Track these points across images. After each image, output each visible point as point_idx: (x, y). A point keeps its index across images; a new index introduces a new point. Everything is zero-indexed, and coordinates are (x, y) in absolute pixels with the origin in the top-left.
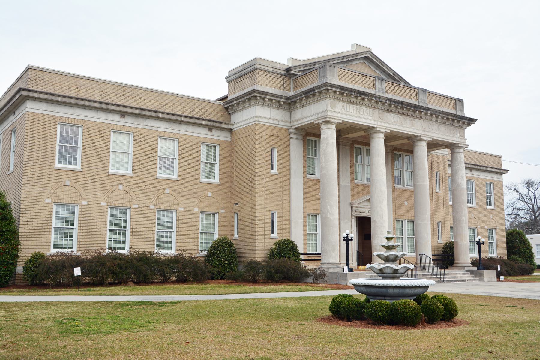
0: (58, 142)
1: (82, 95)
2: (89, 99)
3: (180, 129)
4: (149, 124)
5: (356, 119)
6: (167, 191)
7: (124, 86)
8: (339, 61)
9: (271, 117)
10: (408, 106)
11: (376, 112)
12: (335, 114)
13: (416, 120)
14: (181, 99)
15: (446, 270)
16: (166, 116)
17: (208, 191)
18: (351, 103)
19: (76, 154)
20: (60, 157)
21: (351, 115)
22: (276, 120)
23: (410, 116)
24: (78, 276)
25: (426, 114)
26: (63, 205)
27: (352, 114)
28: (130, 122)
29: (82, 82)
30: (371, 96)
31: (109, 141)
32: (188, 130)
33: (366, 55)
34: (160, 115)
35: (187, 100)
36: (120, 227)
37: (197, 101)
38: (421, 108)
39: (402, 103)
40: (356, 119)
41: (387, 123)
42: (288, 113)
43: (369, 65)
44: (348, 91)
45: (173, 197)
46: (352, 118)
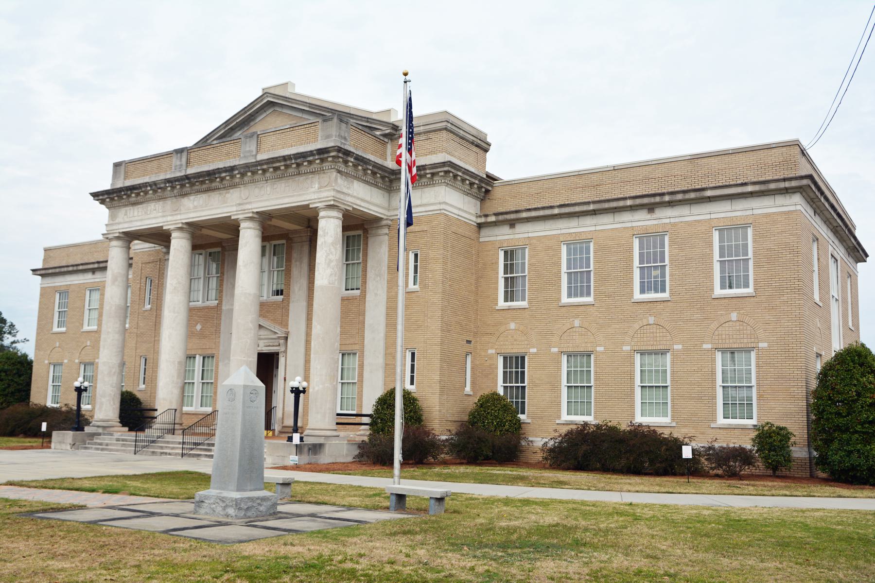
0: (564, 268)
5: (139, 223)
10: (199, 177)
11: (169, 202)
13: (231, 191)
15: (139, 434)
18: (134, 204)
19: (746, 269)
25: (232, 177)
26: (650, 353)
29: (71, 249)
33: (265, 101)
36: (517, 382)
38: (220, 173)
40: (139, 223)
42: (386, 195)
43: (257, 120)
44: (116, 192)
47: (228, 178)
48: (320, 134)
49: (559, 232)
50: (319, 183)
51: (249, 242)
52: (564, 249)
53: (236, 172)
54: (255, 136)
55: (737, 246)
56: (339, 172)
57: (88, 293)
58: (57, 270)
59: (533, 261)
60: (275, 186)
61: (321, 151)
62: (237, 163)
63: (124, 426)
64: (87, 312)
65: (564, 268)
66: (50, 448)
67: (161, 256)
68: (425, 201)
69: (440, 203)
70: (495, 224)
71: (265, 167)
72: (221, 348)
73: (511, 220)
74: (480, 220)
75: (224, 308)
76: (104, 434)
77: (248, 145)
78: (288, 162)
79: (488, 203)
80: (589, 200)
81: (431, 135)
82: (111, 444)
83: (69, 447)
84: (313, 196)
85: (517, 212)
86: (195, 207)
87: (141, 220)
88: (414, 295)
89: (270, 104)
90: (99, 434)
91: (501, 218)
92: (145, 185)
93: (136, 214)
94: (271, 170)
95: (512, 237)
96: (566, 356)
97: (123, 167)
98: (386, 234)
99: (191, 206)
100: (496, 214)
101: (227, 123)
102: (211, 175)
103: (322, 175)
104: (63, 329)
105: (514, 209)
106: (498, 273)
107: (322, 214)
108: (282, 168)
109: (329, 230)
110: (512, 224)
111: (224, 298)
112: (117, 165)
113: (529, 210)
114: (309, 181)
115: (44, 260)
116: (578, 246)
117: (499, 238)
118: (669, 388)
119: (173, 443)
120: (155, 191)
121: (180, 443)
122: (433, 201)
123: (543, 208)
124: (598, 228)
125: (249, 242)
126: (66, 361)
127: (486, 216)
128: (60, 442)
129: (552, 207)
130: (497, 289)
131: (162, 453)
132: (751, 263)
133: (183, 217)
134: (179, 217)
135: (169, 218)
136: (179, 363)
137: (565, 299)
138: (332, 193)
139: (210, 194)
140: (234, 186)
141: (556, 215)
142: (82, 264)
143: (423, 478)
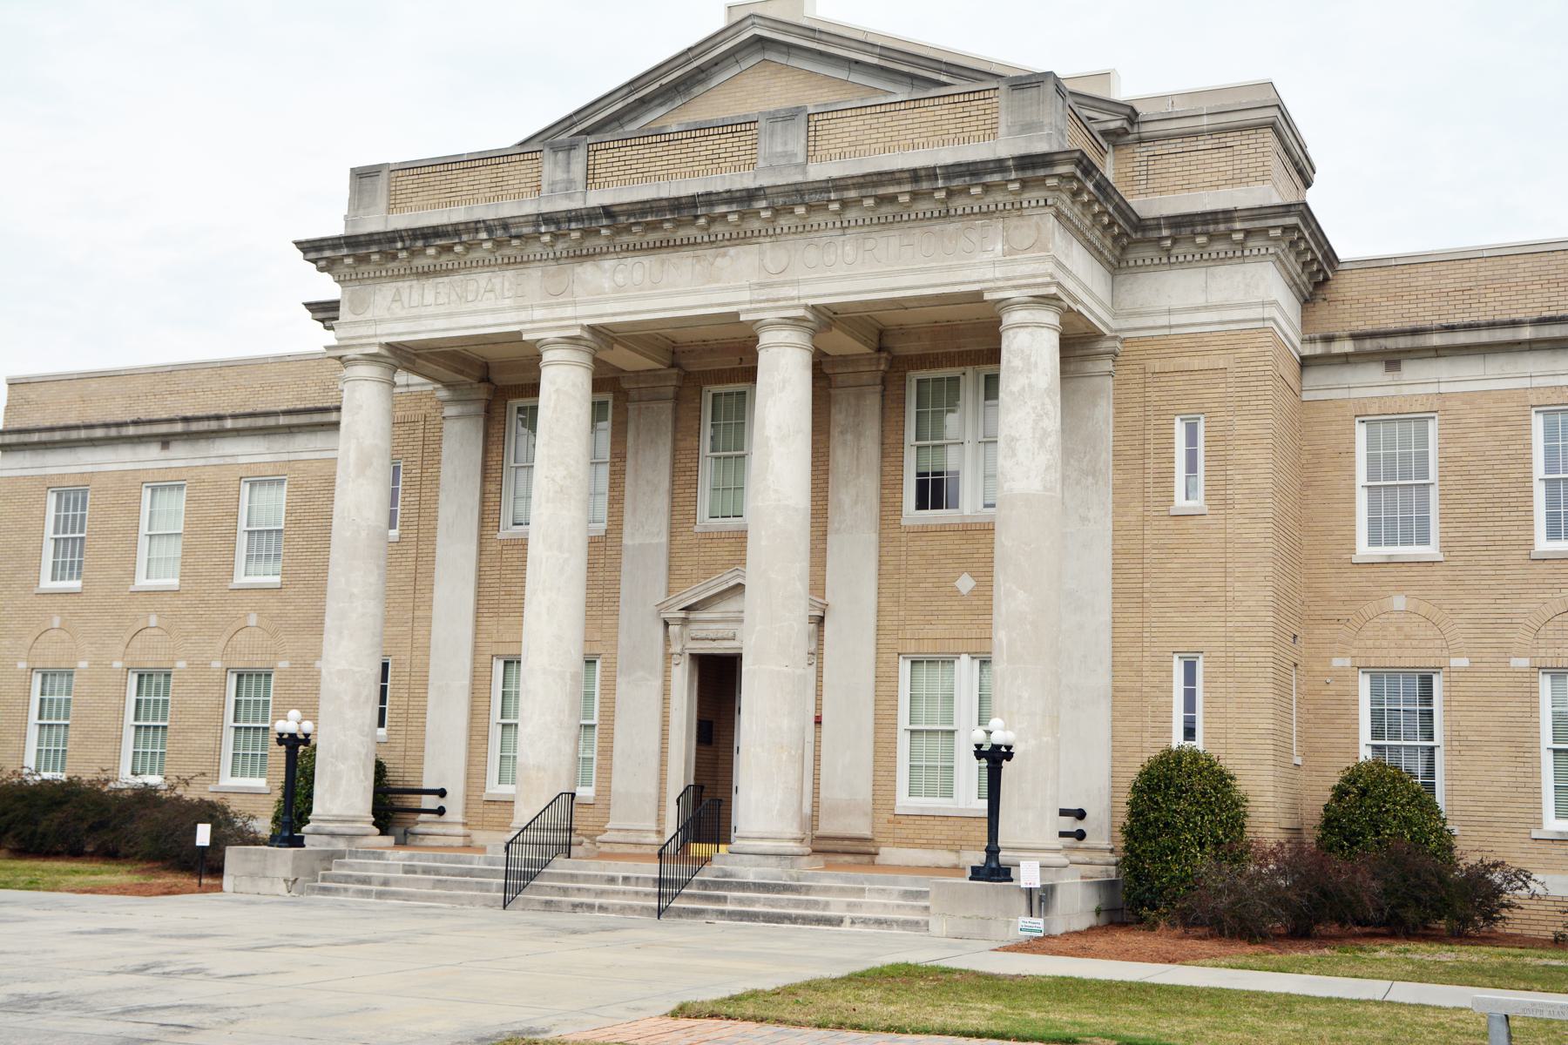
0: (1361, 477)
1: (94, 416)
2: (62, 423)
4: (221, 452)
5: (441, 323)
6: (253, 620)
7: (171, 371)
8: (875, 61)
10: (644, 213)
12: (363, 331)
13: (732, 251)
16: (241, 423)
19: (1424, 506)
20: (1373, 523)
21: (419, 317)
27: (423, 311)
28: (181, 457)
29: (94, 384)
30: (468, 231)
32: (311, 446)
34: (229, 424)
38: (711, 204)
39: (608, 212)
40: (413, 326)
41: (575, 303)
43: (714, 83)
44: (379, 242)
47: (732, 218)
48: (1004, 120)
49: (1526, 383)
50: (1006, 240)
51: (564, 389)
52: (1538, 423)
53: (764, 204)
54: (803, 117)
55: (1405, 457)
56: (1059, 215)
57: (147, 494)
58: (57, 436)
59: (1453, 450)
60: (870, 244)
61: (1026, 162)
62: (764, 181)
63: (383, 833)
64: (143, 543)
65: (1361, 477)
66: (220, 888)
67: (427, 407)
68: (1215, 298)
69: (1263, 304)
70: (1346, 359)
71: (852, 194)
72: (623, 640)
73: (1390, 350)
74: (1308, 350)
75: (627, 541)
76: (354, 854)
77: (778, 139)
78: (925, 185)
79: (1322, 310)
81: (1229, 139)
82: (398, 881)
83: (281, 888)
84: (989, 273)
85: (1415, 332)
86: (619, 288)
87: (450, 315)
88: (1190, 522)
89: (760, 43)
90: (340, 855)
91: (1369, 345)
92: (474, 227)
93: (416, 296)
94: (870, 202)
95: (1392, 391)
97: (382, 181)
98: (1110, 374)
99: (607, 284)
100: (1355, 337)
101: (634, 85)
102: (683, 209)
104: (75, 584)
106: (1353, 477)
107: (1010, 318)
108: (904, 199)
109: (1030, 350)
110: (1393, 361)
111: (627, 517)
112: (362, 176)
113: (1451, 328)
114: (974, 236)
115: (8, 408)
117: (1355, 393)
119: (587, 878)
120: (499, 244)
122: (1239, 297)
123: (1492, 325)
125: (564, 389)
126: (83, 664)
127: (1329, 339)
128: (252, 876)
129: (1515, 324)
130: (1352, 514)
131: (575, 906)
132: (1434, 494)
133: (581, 310)
134: (569, 311)
135: (538, 314)
136: (574, 677)
137: (1364, 549)
138: (1050, 267)
139: (664, 256)
140: (742, 239)
142: (136, 423)
143: (1301, 968)
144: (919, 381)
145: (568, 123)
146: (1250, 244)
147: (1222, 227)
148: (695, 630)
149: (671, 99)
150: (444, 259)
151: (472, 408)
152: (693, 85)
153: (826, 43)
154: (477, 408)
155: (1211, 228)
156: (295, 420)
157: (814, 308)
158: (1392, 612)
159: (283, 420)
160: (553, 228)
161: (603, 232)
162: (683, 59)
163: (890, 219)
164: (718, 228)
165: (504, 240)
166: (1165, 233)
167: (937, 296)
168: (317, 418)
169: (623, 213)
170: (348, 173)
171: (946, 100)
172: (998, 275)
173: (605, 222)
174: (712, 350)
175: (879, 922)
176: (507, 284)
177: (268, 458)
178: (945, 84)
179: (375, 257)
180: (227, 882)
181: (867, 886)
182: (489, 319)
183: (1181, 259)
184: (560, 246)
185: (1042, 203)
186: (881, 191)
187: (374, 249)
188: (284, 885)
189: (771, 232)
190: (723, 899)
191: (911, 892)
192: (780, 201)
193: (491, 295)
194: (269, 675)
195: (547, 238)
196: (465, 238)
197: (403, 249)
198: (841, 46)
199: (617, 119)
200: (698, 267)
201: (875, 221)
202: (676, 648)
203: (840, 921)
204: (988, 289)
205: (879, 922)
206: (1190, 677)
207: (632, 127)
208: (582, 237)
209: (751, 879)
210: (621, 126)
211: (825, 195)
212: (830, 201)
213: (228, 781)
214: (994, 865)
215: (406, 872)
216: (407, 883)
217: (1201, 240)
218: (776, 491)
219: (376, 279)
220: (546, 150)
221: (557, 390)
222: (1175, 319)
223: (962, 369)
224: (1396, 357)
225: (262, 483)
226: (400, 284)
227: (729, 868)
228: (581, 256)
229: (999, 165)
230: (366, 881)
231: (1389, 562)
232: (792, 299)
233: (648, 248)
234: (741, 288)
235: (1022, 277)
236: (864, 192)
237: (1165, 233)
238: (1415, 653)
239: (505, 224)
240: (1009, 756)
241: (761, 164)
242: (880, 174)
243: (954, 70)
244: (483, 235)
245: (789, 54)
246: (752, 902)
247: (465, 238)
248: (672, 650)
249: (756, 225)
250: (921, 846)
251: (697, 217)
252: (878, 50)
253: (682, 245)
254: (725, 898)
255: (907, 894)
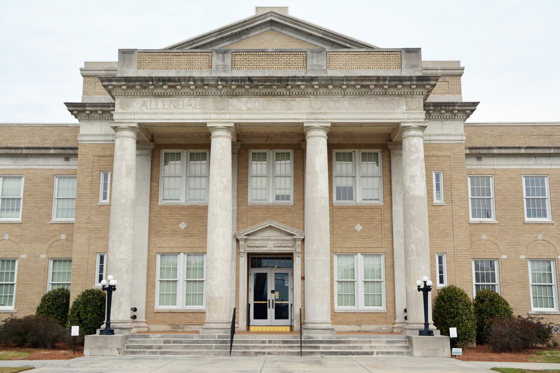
3: (37, 163)
6: (6, 237)
8: (321, 35)
9: (103, 133)
13: (298, 99)
14: (30, 128)
17: (62, 233)
19: (544, 206)
21: (157, 113)
22: (109, 135)
23: (282, 95)
24: (75, 336)
31: (52, 187)
35: (37, 128)
37: (51, 128)
38: (295, 81)
39: (250, 79)
40: (190, 117)
43: (251, 35)
44: (141, 81)
45: (14, 244)
46: (161, 116)
47: (302, 87)
49: (520, 167)
50: (407, 105)
53: (317, 83)
59: (499, 187)
60: (354, 102)
68: (445, 132)
71: (353, 83)
78: (381, 83)
80: (551, 146)
81: (447, 79)
83: (116, 352)
86: (249, 109)
87: (171, 113)
89: (272, 22)
91: (474, 151)
92: (189, 79)
94: (358, 87)
95: (479, 167)
96: (52, 261)
97: (135, 56)
99: (244, 108)
101: (221, 31)
102: (283, 81)
103: (409, 99)
105: (518, 146)
110: (479, 157)
113: (500, 148)
114: (395, 103)
116: (535, 180)
118: (15, 286)
120: (196, 87)
121: (297, 342)
122: (453, 132)
123: (513, 148)
124: (553, 167)
128: (100, 348)
129: (519, 148)
131: (257, 353)
133: (232, 116)
134: (227, 116)
135: (213, 116)
140: (303, 95)
141: (522, 154)
144: (165, 153)
145: (191, 43)
146: (91, 115)
147: (451, 108)
148: (249, 243)
149: (233, 39)
150: (169, 91)
151: (145, 152)
152: (243, 35)
153: (301, 26)
154: (149, 152)
155: (447, 108)
156: (31, 152)
157: (139, 124)
158: (481, 240)
159: (24, 151)
160: (224, 83)
161: (246, 87)
162: (242, 24)
163: (363, 93)
164: (295, 90)
165: (200, 86)
166: (431, 108)
167: (380, 123)
168: (43, 151)
169: (256, 80)
170: (117, 51)
171: (381, 53)
172: (405, 117)
173: (248, 83)
174: (254, 136)
175: (388, 353)
176: (197, 103)
177: (14, 167)
178: (346, 47)
179: (138, 87)
180: (86, 351)
181: (372, 340)
182: (190, 117)
183: (434, 117)
184: (224, 90)
185: (421, 93)
186: (364, 83)
187: (138, 83)
188: (117, 351)
189: (315, 94)
190: (319, 347)
191: (391, 341)
192: (323, 82)
193: (190, 107)
194: (14, 261)
195: (220, 87)
196: (183, 83)
197: (153, 85)
198: (307, 28)
199: (210, 44)
200: (283, 104)
201: (358, 94)
202: (242, 250)
203: (372, 353)
204: (403, 122)
205: (388, 353)
206: (441, 262)
207: (217, 47)
208: (236, 88)
209: (320, 339)
210: (211, 47)
211: (342, 82)
212: (343, 84)
213: (534, 310)
214: (109, 329)
215: (165, 343)
216: (166, 347)
217: (443, 112)
218: (321, 191)
219: (134, 96)
220: (214, 52)
221: (222, 147)
222: (432, 138)
223: (354, 150)
224: (480, 156)
225: (10, 178)
226: (145, 99)
227: (310, 335)
228: (233, 95)
229: (410, 79)
230: (150, 347)
231: (481, 224)
232: (324, 119)
233: (263, 95)
234: (303, 114)
235: (413, 119)
236: (357, 83)
237: (431, 108)
238: (490, 253)
239: (202, 79)
240: (115, 289)
241: (308, 68)
242: (365, 77)
243: (352, 43)
244: (192, 83)
245: (282, 28)
246: (330, 348)
247: (183, 83)
248: (240, 251)
249: (310, 90)
250: (345, 324)
251: (288, 85)
252: (323, 32)
253: (278, 95)
254: (319, 347)
255: (388, 342)
